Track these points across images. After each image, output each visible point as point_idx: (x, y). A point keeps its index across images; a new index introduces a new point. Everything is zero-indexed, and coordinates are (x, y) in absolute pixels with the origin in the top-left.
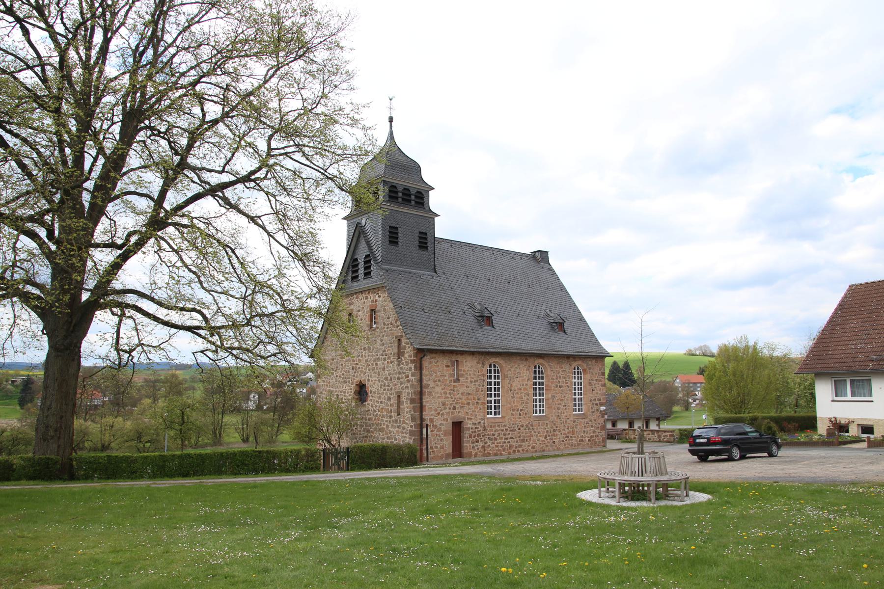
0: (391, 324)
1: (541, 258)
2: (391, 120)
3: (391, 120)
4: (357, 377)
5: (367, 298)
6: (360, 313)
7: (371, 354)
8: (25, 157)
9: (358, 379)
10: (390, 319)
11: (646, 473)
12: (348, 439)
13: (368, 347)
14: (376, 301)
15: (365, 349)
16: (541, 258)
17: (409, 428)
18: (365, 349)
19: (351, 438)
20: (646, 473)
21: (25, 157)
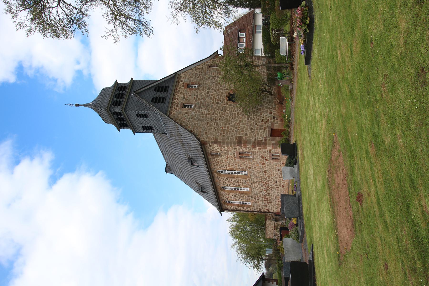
0: (200, 72)
1: (168, 169)
2: (77, 105)
3: (77, 105)
4: (223, 99)
5: (179, 91)
6: (186, 98)
7: (212, 87)
8: (110, 7)
9: (225, 98)
10: (197, 73)
11: (308, 61)
12: (261, 108)
13: (207, 90)
14: (183, 84)
15: (208, 93)
16: (168, 169)
17: (256, 60)
18: (208, 93)
19: (261, 106)
20: (308, 61)
21: (110, 7)
